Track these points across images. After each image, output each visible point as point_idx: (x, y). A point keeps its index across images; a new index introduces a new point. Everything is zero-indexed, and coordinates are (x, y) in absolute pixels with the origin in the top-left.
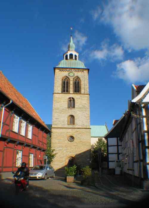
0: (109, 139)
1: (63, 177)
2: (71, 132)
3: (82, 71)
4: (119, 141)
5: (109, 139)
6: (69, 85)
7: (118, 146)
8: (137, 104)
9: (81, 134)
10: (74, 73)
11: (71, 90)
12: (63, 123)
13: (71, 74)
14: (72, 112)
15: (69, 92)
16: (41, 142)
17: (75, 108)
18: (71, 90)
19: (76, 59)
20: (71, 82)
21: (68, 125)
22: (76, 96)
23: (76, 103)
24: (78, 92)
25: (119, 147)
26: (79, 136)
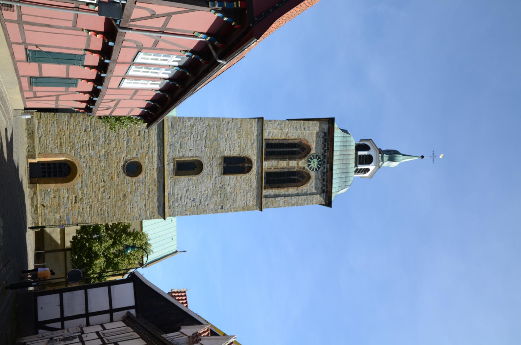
0: (131, 285)
1: (38, 258)
2: (150, 167)
3: (323, 188)
4: (125, 312)
5: (131, 285)
6: (287, 156)
7: (111, 311)
8: (25, 343)
9: (147, 193)
10: (320, 170)
11: (270, 165)
12: (178, 145)
13: (315, 160)
14: (212, 168)
15: (266, 159)
16: (116, 105)
17: (222, 176)
18: (270, 165)
19: (358, 171)
20: (293, 164)
21: (174, 159)
22: (252, 176)
23: (281, 137)
24: (267, 182)
25: (108, 316)
26: (141, 189)
